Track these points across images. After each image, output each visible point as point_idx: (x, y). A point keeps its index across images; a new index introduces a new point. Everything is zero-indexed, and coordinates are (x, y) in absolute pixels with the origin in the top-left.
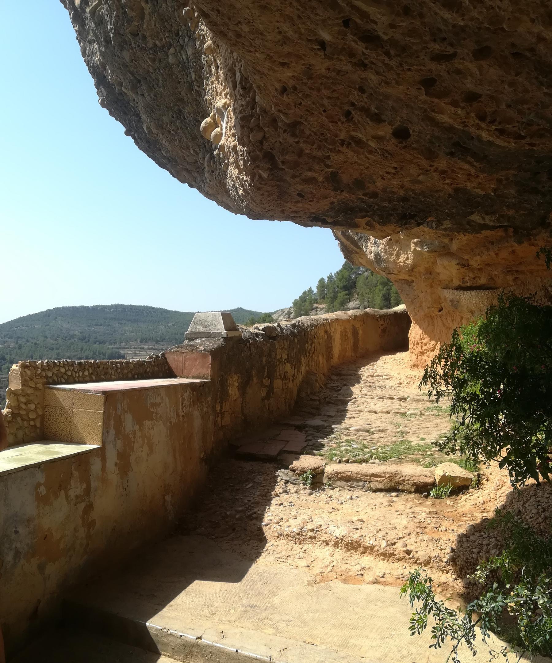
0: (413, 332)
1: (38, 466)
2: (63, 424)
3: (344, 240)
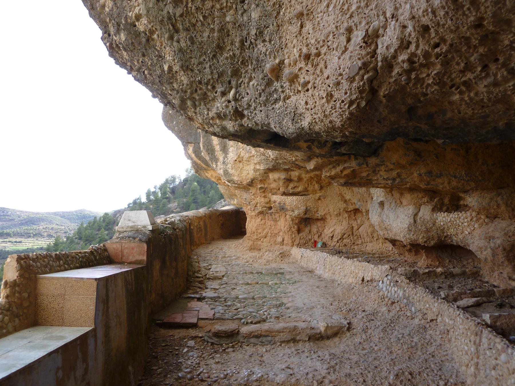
0: (250, 225)
1: (56, 351)
2: (54, 310)
3: (195, 159)
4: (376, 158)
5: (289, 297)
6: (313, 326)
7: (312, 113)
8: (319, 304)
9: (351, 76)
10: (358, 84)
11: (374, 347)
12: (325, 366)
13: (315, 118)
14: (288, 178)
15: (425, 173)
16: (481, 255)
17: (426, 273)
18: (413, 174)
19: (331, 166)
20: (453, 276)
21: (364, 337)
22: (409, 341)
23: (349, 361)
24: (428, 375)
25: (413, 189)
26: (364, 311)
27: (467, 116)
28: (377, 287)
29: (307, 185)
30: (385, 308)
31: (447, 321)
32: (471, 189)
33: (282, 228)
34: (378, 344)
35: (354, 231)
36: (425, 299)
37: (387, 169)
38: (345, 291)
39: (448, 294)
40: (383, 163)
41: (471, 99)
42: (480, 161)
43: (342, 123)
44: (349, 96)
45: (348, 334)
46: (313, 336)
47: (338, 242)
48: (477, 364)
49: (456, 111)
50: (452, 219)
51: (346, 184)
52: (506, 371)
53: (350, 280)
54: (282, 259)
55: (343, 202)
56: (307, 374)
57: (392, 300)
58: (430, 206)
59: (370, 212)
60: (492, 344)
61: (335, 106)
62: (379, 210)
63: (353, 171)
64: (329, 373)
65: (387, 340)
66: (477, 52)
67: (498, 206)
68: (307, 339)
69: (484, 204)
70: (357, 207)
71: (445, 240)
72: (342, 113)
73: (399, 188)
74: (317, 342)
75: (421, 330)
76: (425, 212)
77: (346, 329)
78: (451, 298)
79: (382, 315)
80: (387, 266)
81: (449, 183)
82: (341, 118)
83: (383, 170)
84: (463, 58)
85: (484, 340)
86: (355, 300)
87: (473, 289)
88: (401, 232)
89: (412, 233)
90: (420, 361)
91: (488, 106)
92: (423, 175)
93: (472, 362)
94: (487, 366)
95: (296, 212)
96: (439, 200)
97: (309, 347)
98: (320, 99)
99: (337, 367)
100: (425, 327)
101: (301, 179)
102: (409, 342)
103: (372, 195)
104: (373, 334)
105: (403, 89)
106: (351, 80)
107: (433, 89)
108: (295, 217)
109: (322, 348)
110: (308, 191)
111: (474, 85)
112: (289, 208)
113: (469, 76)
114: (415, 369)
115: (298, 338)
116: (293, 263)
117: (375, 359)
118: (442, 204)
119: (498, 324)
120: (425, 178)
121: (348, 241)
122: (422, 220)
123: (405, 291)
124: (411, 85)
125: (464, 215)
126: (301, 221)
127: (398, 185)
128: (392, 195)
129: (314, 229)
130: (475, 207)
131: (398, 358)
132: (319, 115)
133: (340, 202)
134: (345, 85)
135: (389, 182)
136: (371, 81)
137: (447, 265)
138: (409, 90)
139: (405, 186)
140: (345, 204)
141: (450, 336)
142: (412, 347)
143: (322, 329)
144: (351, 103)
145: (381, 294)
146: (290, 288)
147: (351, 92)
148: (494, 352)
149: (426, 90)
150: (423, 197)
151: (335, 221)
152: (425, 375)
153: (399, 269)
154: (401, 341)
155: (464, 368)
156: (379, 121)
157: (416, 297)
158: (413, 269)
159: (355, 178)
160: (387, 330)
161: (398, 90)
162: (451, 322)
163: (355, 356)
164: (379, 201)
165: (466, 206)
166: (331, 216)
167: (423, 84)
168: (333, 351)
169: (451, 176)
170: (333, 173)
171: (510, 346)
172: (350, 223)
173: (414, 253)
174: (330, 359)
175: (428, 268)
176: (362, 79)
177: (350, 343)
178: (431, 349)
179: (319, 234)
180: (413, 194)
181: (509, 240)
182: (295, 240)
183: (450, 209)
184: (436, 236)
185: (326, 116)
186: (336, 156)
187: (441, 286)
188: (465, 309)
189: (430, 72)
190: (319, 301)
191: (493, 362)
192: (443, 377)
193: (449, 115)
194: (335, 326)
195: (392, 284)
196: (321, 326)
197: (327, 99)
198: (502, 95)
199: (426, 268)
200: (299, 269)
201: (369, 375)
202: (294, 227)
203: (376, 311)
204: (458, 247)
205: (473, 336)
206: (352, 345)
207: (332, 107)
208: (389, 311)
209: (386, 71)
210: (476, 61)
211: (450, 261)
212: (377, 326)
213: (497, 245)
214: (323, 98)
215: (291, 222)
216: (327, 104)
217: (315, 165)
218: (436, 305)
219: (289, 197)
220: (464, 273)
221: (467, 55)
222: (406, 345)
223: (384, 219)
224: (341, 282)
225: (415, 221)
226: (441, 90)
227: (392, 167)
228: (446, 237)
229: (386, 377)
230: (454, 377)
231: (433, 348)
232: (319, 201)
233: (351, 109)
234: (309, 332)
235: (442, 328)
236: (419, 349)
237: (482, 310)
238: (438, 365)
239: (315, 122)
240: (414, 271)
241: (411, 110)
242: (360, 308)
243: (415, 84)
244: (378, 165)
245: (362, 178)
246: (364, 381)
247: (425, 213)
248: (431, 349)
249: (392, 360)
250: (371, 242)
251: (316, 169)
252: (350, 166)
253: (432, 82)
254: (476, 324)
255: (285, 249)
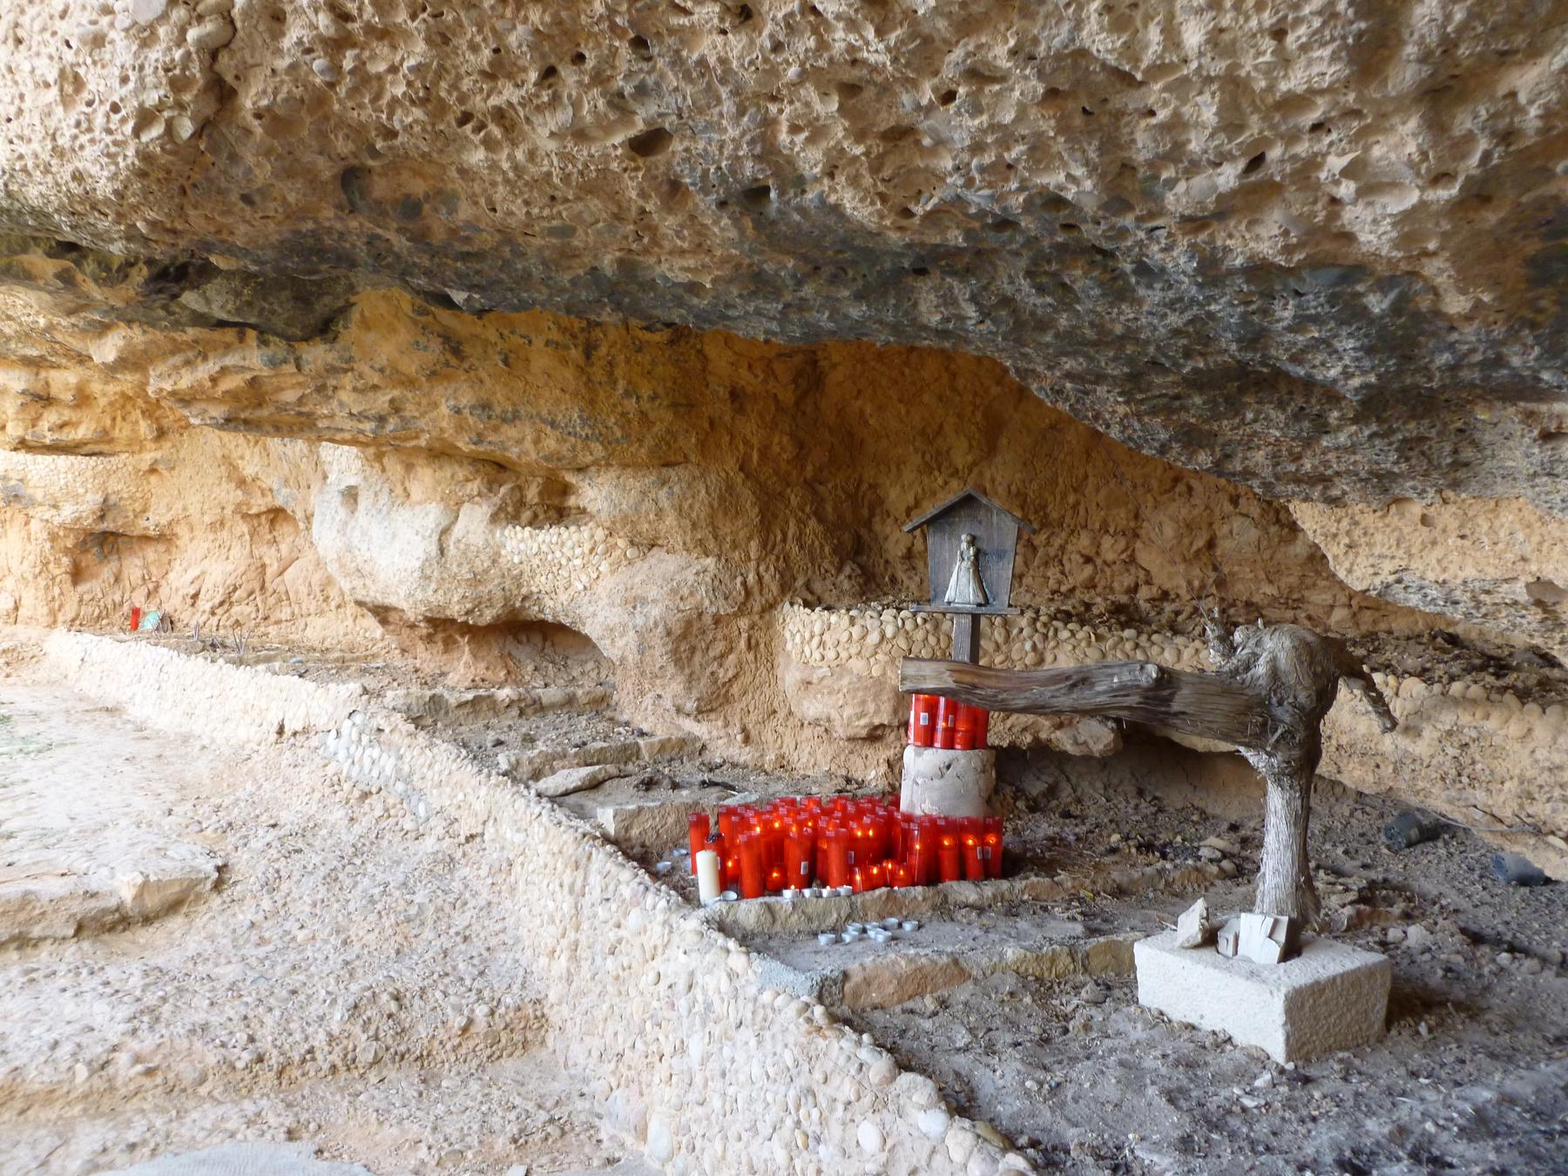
4: (328, 346)
5: (16, 798)
6: (94, 887)
7: (11, 135)
8: (126, 814)
9: (142, 21)
10: (165, 55)
11: (295, 932)
12: (124, 1011)
13: (21, 157)
14: (38, 388)
15: (473, 408)
16: (611, 649)
17: (466, 703)
18: (436, 405)
19: (178, 359)
20: (540, 708)
21: (266, 904)
22: (401, 902)
23: (208, 986)
24: (445, 994)
25: (440, 453)
26: (274, 826)
27: (512, 222)
28: (321, 751)
29: (108, 422)
30: (342, 813)
31: (508, 835)
32: (595, 463)
33: (14, 564)
34: (309, 923)
35: (268, 578)
36: (456, 777)
37: (359, 385)
38: (221, 766)
39: (518, 762)
40: (347, 366)
41: (516, 168)
42: (621, 385)
43: (118, 185)
44: (136, 92)
45: (216, 901)
46: (93, 919)
47: (213, 614)
48: (576, 945)
49: (482, 201)
50: (544, 548)
51: (232, 425)
52: (637, 952)
53: (242, 733)
54: (8, 670)
55: (233, 485)
56: (55, 1045)
57: (362, 786)
58: (485, 507)
59: (316, 521)
60: (611, 888)
61: (89, 121)
62: (343, 513)
63: (253, 382)
64: (134, 1031)
65: (336, 906)
66: (526, 20)
67: (660, 513)
68: (71, 932)
69: (624, 506)
70: (279, 502)
71: (523, 607)
72: (113, 149)
73: (397, 449)
74: (106, 937)
75: (439, 869)
76: (473, 522)
77: (209, 885)
78: (525, 769)
79: (330, 833)
80: (354, 687)
81: (537, 441)
82: (113, 168)
83: (349, 387)
84: (486, 30)
85: (595, 880)
86: (252, 795)
87: (585, 744)
88: (401, 582)
89: (433, 586)
90: (426, 957)
91: (566, 200)
92: (466, 412)
93: (564, 942)
94: (598, 947)
95: (67, 512)
96: (512, 489)
97: (78, 956)
98: (37, 85)
99: (166, 1010)
100: (452, 860)
101: (87, 398)
102: (402, 905)
103: (326, 467)
104: (295, 895)
105: (318, 100)
106: (145, 36)
107: (410, 119)
108: (61, 526)
109: (124, 954)
110: (112, 441)
111: (526, 127)
112: (39, 495)
113: (508, 94)
114: (410, 981)
115: (36, 931)
116: (51, 683)
117: (294, 968)
118: (521, 504)
119: (635, 832)
120: (471, 420)
121: (248, 609)
122: (462, 546)
123: (401, 757)
124: (342, 90)
125: (575, 537)
126: (84, 542)
127: (395, 438)
128: (384, 470)
129: (133, 568)
130: (604, 516)
131: (366, 957)
132: (35, 146)
133: (224, 485)
134: (122, 50)
135: (368, 426)
136: (212, 52)
137: (527, 678)
138: (336, 107)
139: (413, 443)
140: (239, 492)
141: (512, 879)
142: (408, 920)
143: (127, 895)
144: (145, 118)
145: (330, 770)
146: (27, 767)
147: (141, 79)
148: (614, 907)
149: (390, 118)
150: (468, 480)
151: (206, 545)
152: (438, 995)
153: (390, 694)
154: (379, 906)
155: (543, 961)
156: (246, 199)
157: (429, 775)
158: (429, 693)
159: (260, 405)
160: (341, 876)
161: (302, 100)
162: (519, 838)
163: (230, 967)
164: (343, 487)
165: (583, 511)
166: (192, 530)
167: (377, 97)
168: (160, 961)
169: (544, 421)
170: (186, 381)
171: (652, 889)
172: (256, 552)
173: (440, 646)
174: (145, 988)
175: (476, 687)
176: (181, 40)
177: (220, 929)
178: (460, 920)
179: (151, 586)
180: (441, 468)
181: (682, 607)
182: (61, 606)
183: (541, 517)
184: (499, 594)
185: (58, 152)
186: (194, 326)
187: (502, 738)
188: (557, 799)
189: (398, 58)
190: (128, 806)
191: (611, 935)
192: (486, 993)
193: (465, 212)
194: (171, 882)
195: (365, 739)
196: (123, 887)
197: (61, 90)
198: (598, 170)
199: (468, 689)
200: (69, 704)
201: (269, 1020)
202: (58, 562)
203: (311, 824)
204: (559, 628)
205: (568, 871)
206: (228, 933)
207: (78, 124)
208: (352, 819)
209: (261, 28)
210: (525, 48)
211: (536, 669)
212: (310, 868)
213: (651, 622)
214: (47, 85)
215: (48, 545)
216: (60, 108)
217: (121, 351)
218: (483, 791)
219: (39, 458)
220: (570, 701)
221: (499, 25)
222: (392, 916)
223: (355, 542)
224: (213, 741)
225: (442, 551)
226: (433, 125)
227: (376, 381)
228: (525, 598)
229: (322, 1018)
230: (515, 988)
231: (468, 914)
232: (153, 479)
233: (145, 138)
234: (78, 908)
235: (495, 856)
236: (430, 922)
237: (601, 799)
238: (475, 961)
239: (25, 170)
240: (432, 697)
241: (351, 177)
242: (264, 818)
243: (354, 91)
244: (332, 370)
245: (282, 408)
246: (252, 1039)
247: (472, 528)
248: (460, 920)
249: (347, 963)
250: (321, 613)
251: (124, 363)
252: (242, 363)
253: (404, 94)
254: (579, 836)
255: (23, 638)
